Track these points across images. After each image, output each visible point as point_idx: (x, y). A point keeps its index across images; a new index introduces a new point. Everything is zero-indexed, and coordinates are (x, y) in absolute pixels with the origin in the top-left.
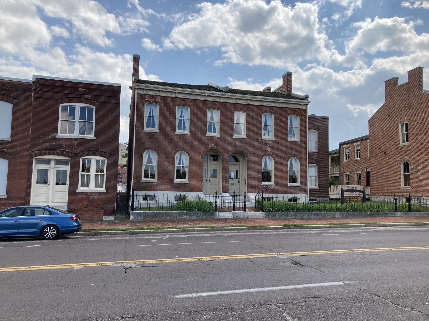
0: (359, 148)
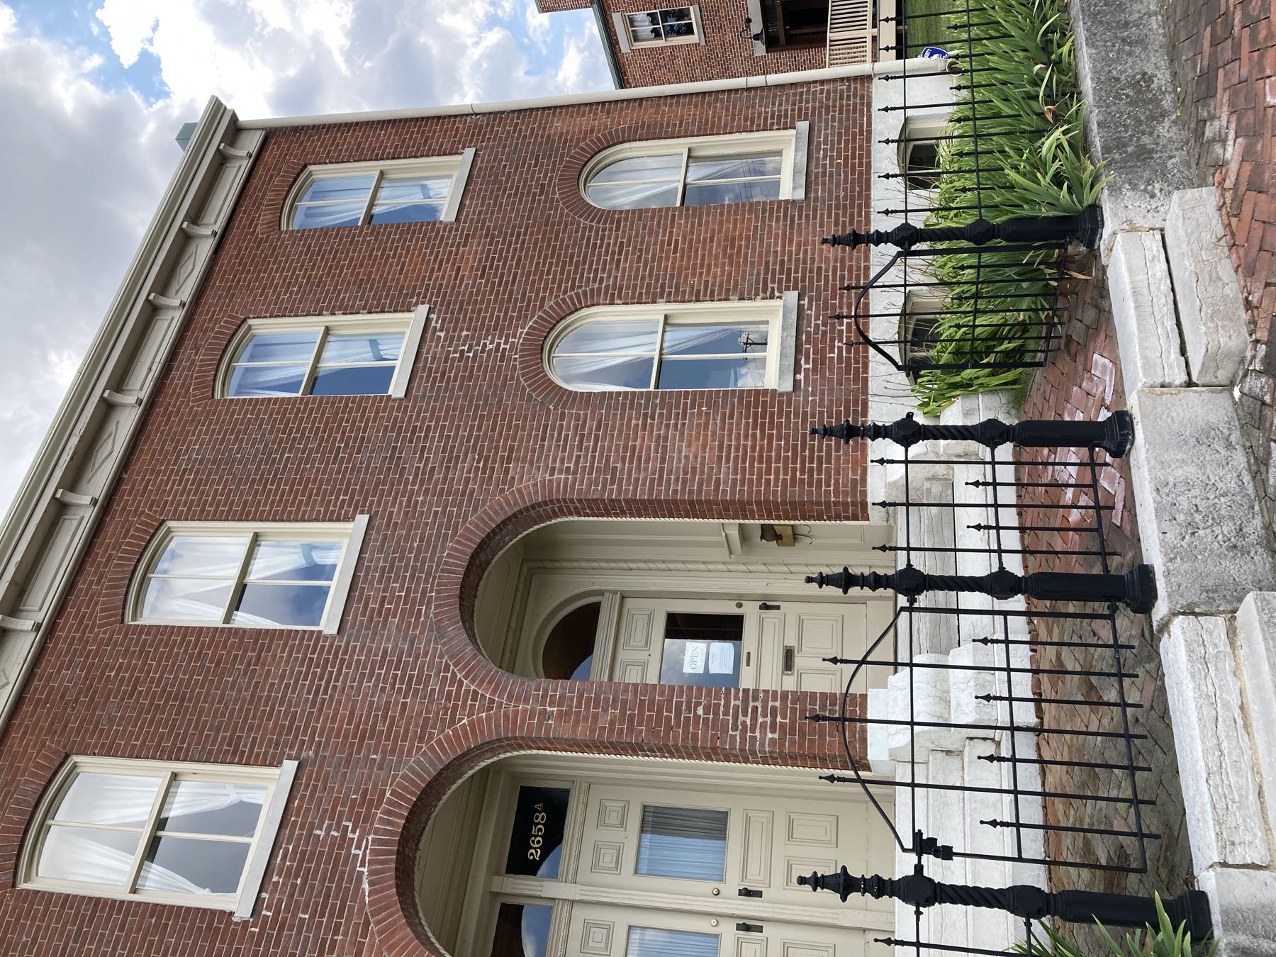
0: (645, 27)
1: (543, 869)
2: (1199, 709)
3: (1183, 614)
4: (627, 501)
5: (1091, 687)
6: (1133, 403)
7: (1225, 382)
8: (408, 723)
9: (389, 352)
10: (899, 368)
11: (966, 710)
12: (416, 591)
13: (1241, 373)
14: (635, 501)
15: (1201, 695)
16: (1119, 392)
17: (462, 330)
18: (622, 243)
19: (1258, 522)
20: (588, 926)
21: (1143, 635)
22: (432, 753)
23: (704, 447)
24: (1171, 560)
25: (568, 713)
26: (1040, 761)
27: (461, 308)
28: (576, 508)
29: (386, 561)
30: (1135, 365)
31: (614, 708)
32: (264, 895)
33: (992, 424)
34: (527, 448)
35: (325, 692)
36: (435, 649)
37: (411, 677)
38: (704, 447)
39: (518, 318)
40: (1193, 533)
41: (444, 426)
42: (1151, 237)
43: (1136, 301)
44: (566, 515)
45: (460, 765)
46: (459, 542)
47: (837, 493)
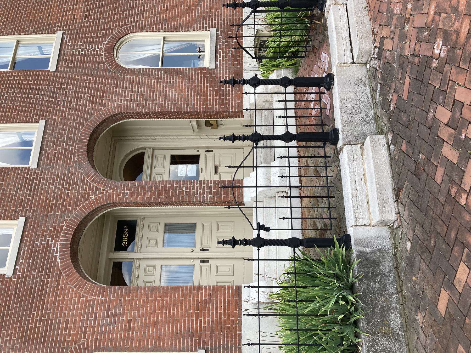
1: (130, 248)
2: (351, 176)
3: (347, 144)
4: (152, 112)
5: (317, 172)
6: (334, 71)
7: (365, 62)
8: (70, 200)
9: (47, 51)
10: (253, 58)
11: (276, 181)
12: (69, 150)
13: (370, 59)
14: (155, 112)
15: (351, 172)
16: (330, 67)
17: (78, 42)
18: (144, 6)
19: (372, 112)
20: (146, 267)
21: (334, 153)
22: (81, 210)
23: (182, 91)
24: (344, 126)
25: (134, 193)
26: (301, 197)
27: (77, 33)
28: (132, 116)
29: (54, 138)
30: (335, 56)
31: (152, 190)
32: (17, 267)
33: (285, 78)
34: (110, 91)
35: (34, 190)
36: (79, 172)
37: (70, 183)
38: (182, 91)
39: (102, 38)
40: (352, 117)
41: (74, 83)
42: (342, 7)
43: (336, 32)
44: (128, 119)
45: (93, 214)
46: (84, 130)
47: (232, 108)
